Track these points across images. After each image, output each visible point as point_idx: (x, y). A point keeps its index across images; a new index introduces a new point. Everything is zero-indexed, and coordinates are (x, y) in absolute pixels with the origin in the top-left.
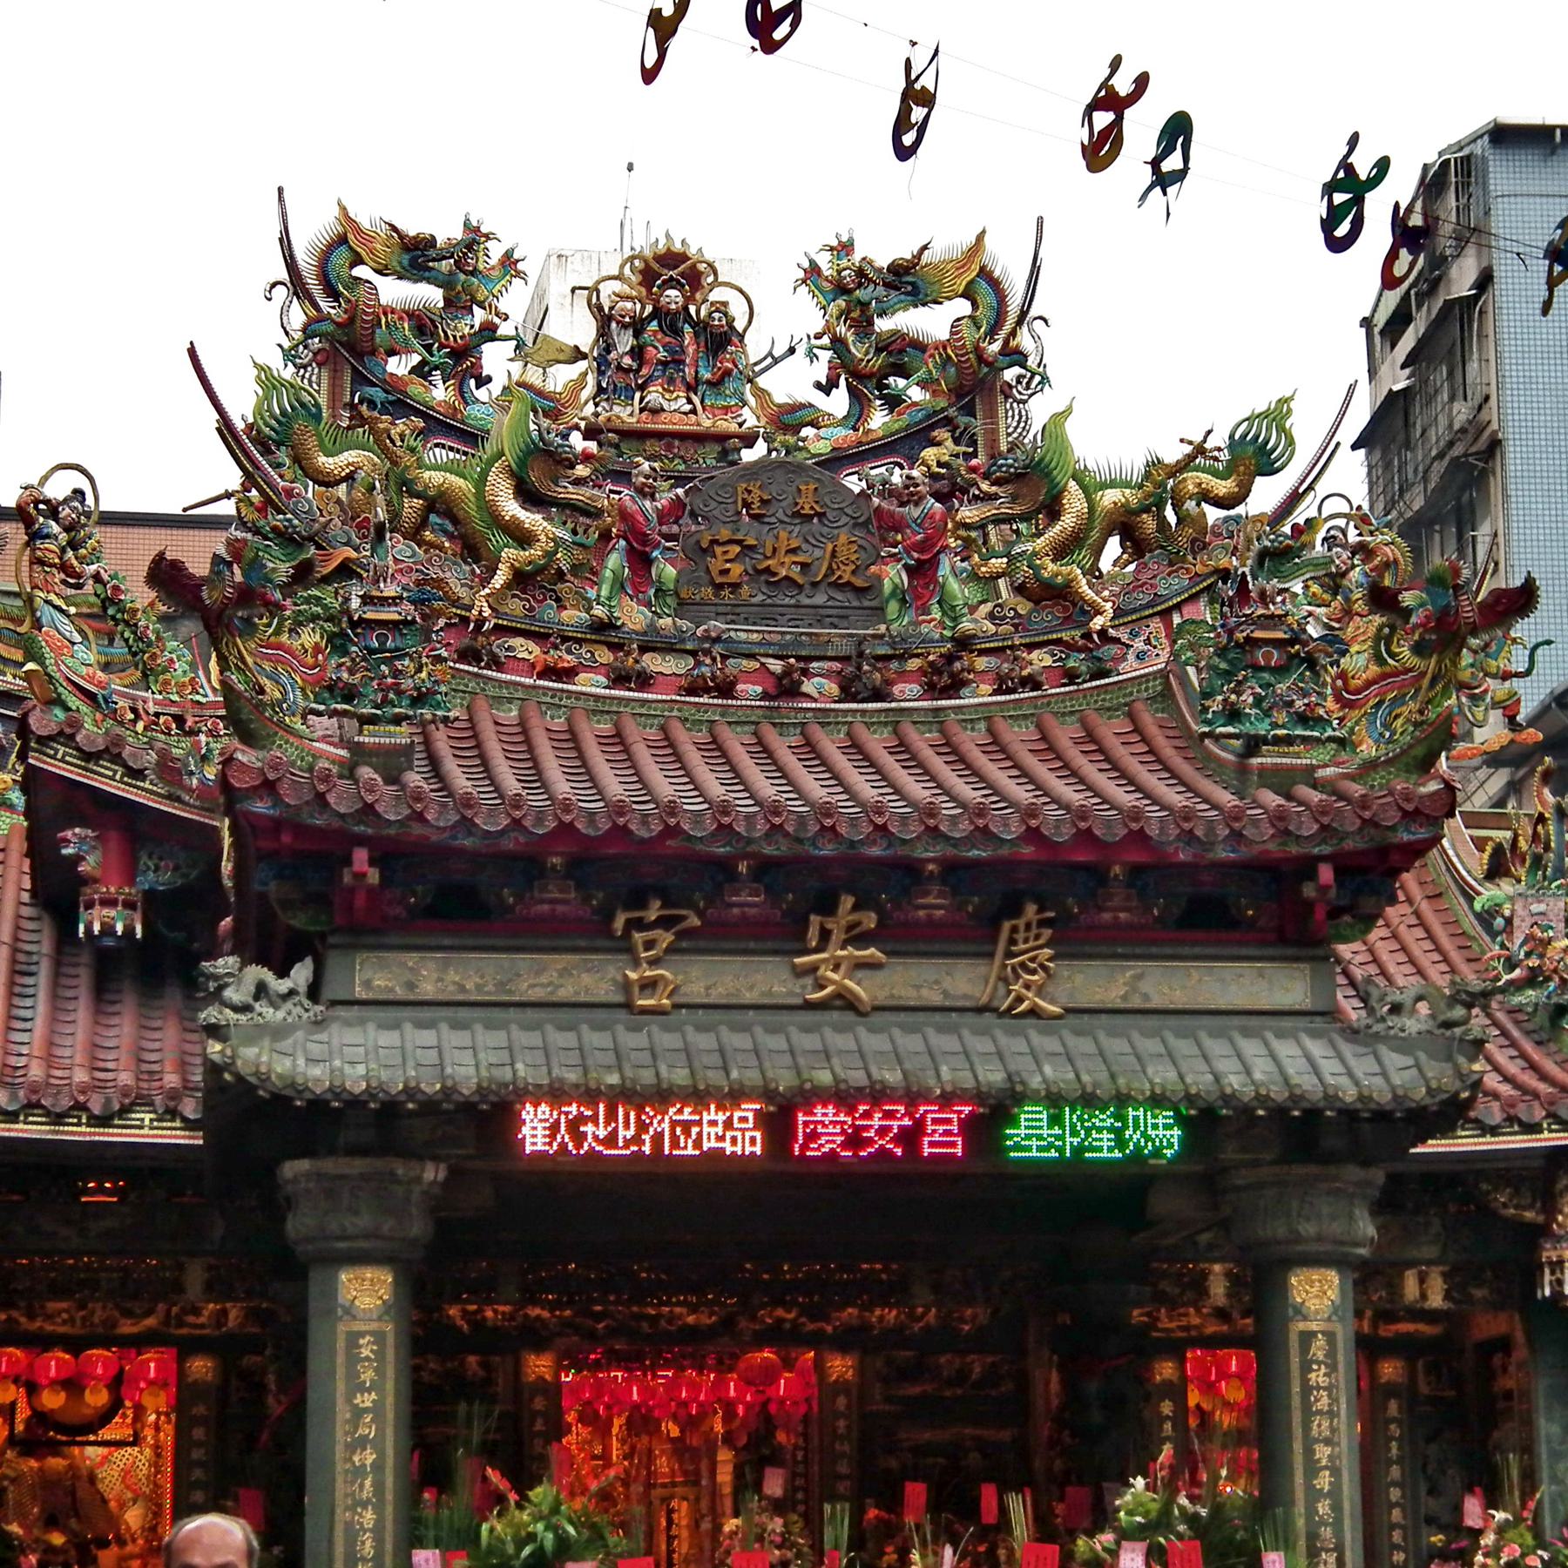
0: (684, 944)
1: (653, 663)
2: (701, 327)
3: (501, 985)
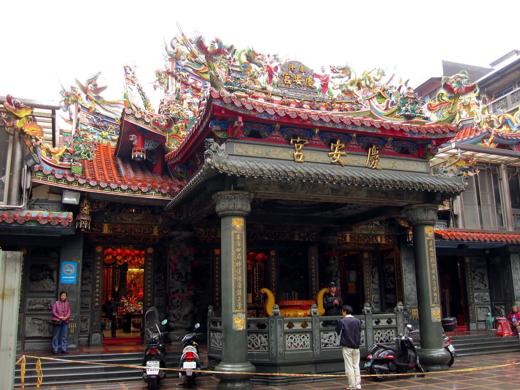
0: (306, 148)
1: (274, 98)
3: (267, 154)
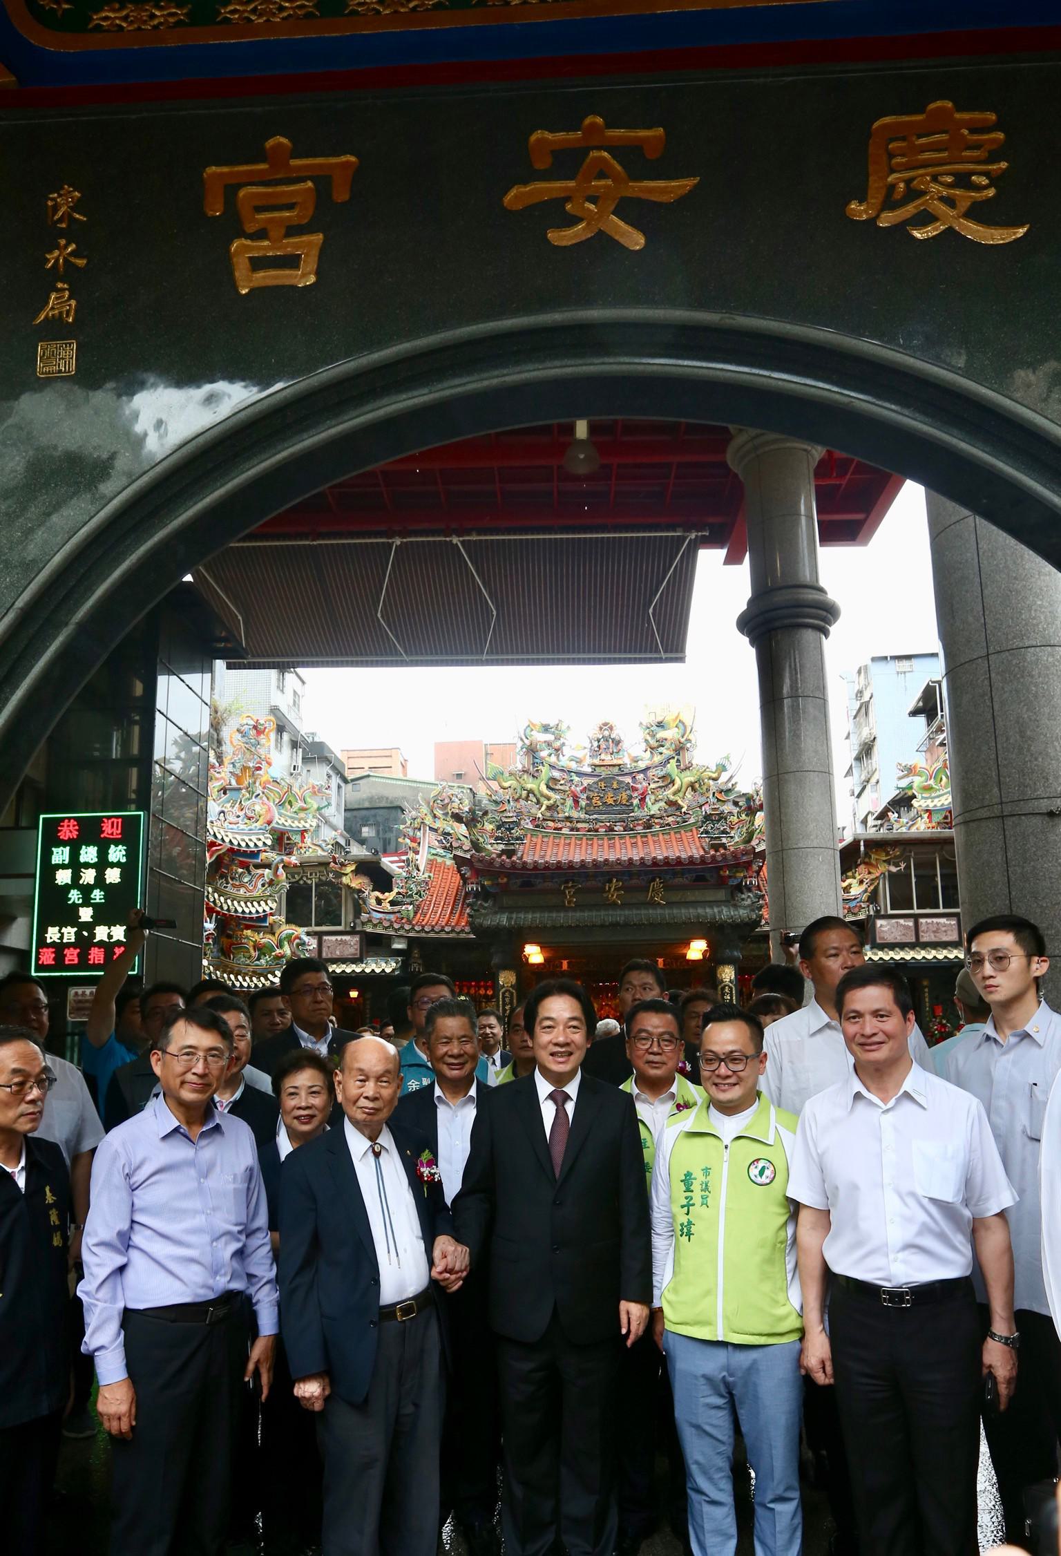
2: (613, 740)
